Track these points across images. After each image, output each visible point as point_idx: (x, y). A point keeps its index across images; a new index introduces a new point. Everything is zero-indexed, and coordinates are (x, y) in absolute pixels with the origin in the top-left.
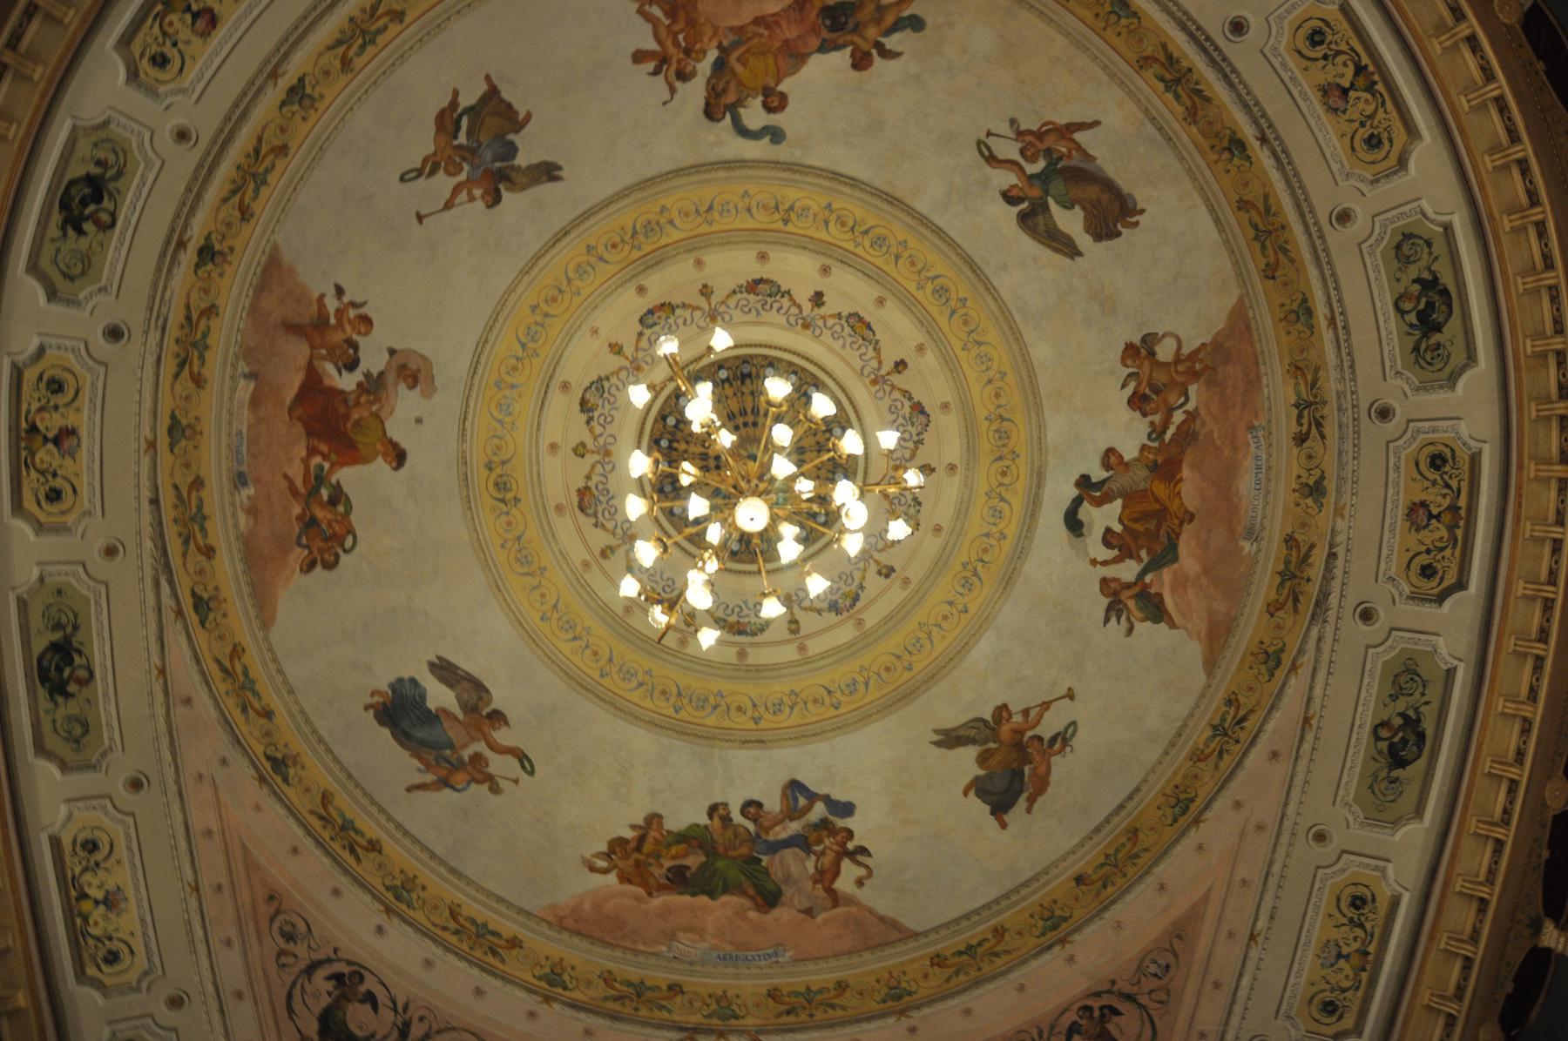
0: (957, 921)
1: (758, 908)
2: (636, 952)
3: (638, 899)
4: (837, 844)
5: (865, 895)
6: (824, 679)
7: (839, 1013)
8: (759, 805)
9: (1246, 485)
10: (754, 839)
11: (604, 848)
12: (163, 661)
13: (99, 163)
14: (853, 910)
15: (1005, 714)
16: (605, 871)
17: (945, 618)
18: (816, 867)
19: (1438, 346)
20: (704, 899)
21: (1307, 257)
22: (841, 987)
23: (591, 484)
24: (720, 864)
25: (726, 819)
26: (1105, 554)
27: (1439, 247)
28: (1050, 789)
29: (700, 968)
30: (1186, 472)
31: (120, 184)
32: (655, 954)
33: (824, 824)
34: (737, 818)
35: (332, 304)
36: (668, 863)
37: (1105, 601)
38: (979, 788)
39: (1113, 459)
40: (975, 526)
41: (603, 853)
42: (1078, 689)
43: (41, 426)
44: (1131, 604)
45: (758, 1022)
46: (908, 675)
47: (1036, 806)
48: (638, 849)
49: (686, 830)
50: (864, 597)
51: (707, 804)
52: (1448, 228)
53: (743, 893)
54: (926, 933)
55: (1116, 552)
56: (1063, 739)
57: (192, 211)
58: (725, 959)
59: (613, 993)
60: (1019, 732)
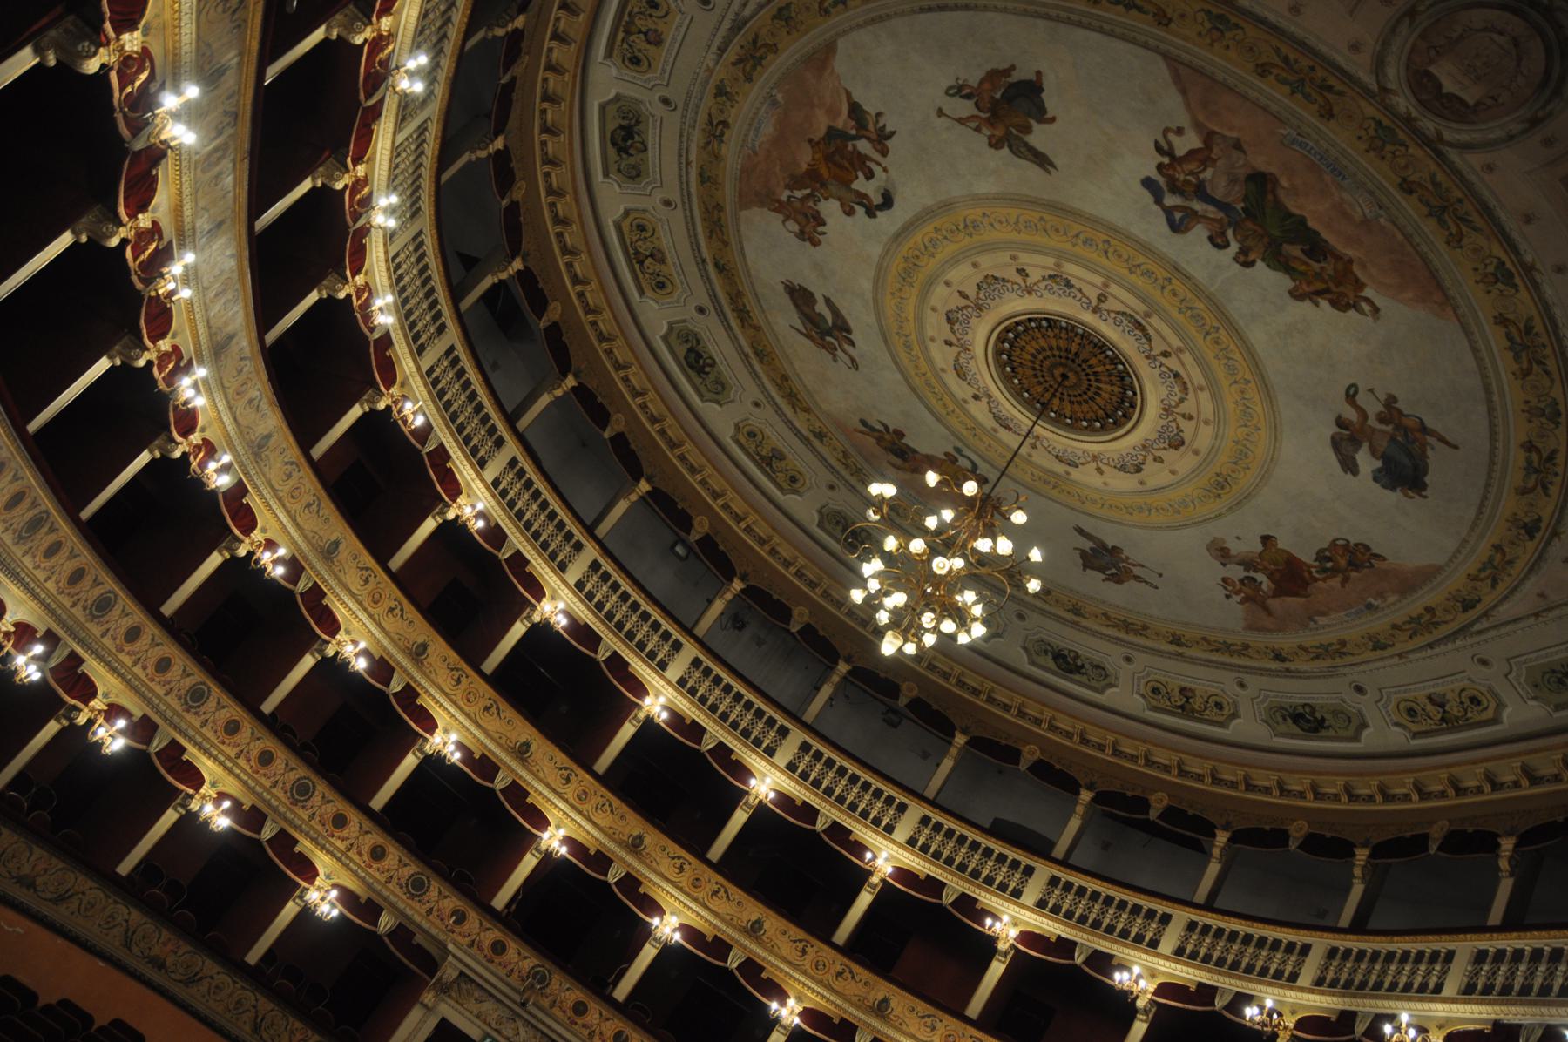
0: (1123, 38)
1: (1275, 182)
2: (1408, 237)
3: (1363, 266)
4: (1175, 169)
5: (1183, 120)
6: (1104, 261)
7: (1285, 50)
8: (1211, 239)
9: (768, 130)
10: (1237, 226)
11: (1352, 313)
12: (1528, 617)
13: (1285, 719)
14: (1201, 118)
15: (994, 141)
16: (1368, 300)
17: (1000, 222)
18: (1205, 169)
19: (624, 118)
20: (1312, 224)
21: (695, 200)
22: (1263, 70)
23: (1166, 445)
24: (1276, 233)
25: (1244, 251)
26: (877, 170)
27: (613, 168)
28: (989, 67)
29: (1369, 184)
30: (804, 167)
31: (1287, 707)
32: (1395, 224)
33: (1175, 188)
34: (1234, 247)
35: (1238, 598)
36: (1316, 266)
37: (889, 143)
38: (1041, 114)
39: (847, 209)
40: (951, 248)
41: (1357, 310)
42: (933, 114)
43: (1439, 716)
44: (871, 127)
45: (1363, 104)
46: (1046, 217)
47: (1005, 66)
48: (1327, 291)
49: (1279, 270)
50: (1047, 273)
51: (1248, 271)
52: (606, 174)
53: (1277, 201)
54: (1156, 50)
55: (868, 163)
56: (959, 91)
57: (1270, 670)
58: (1340, 174)
59: (1464, 229)
60: (991, 123)
